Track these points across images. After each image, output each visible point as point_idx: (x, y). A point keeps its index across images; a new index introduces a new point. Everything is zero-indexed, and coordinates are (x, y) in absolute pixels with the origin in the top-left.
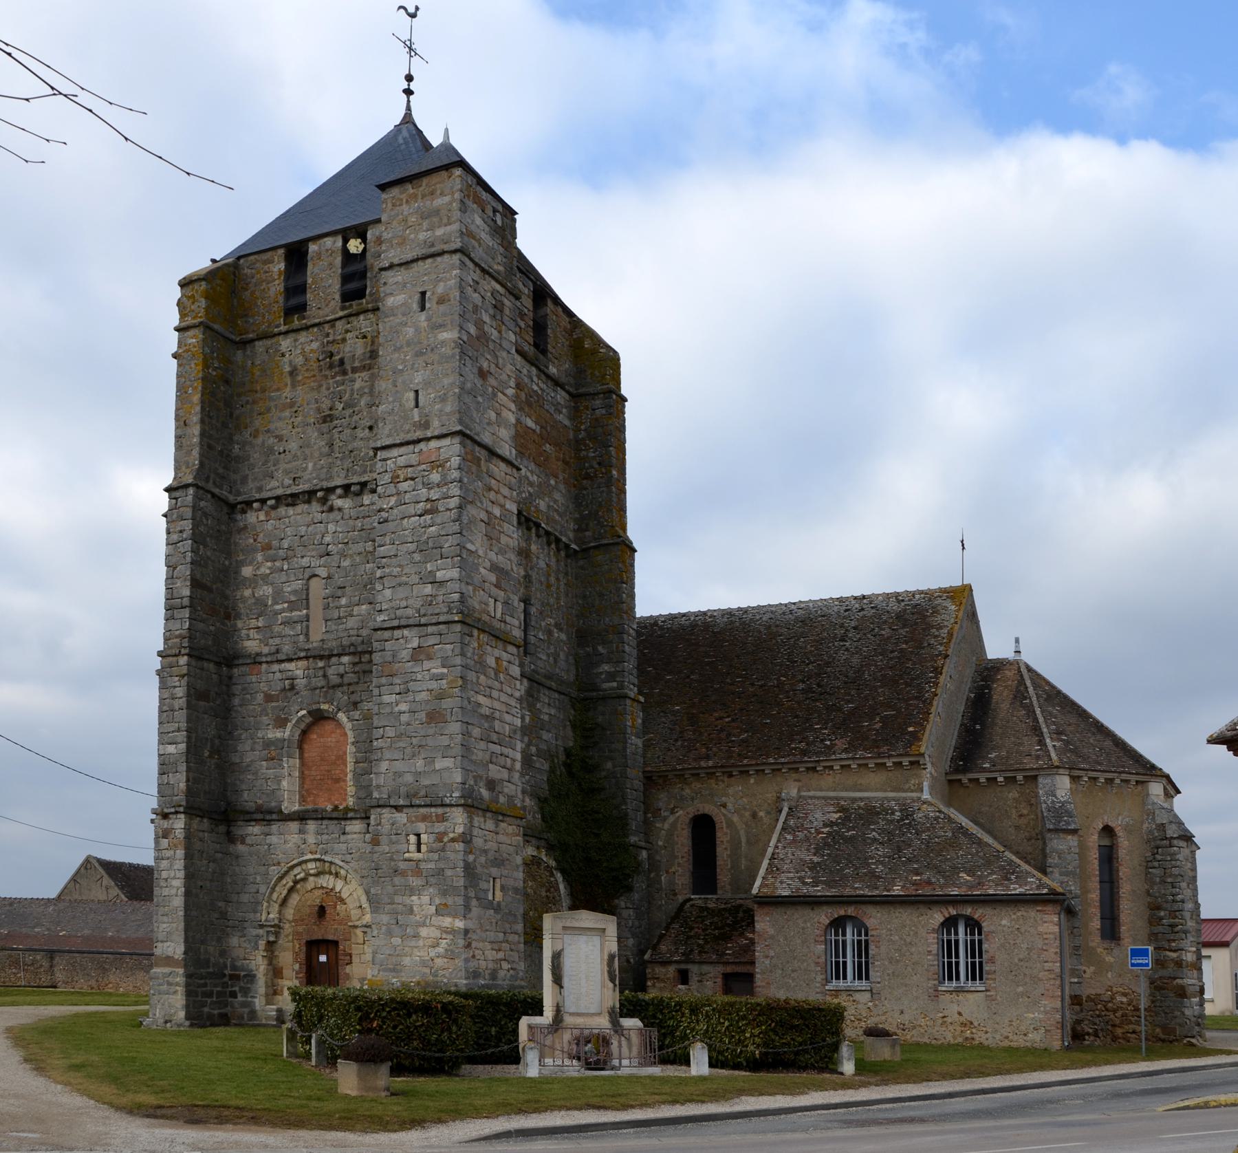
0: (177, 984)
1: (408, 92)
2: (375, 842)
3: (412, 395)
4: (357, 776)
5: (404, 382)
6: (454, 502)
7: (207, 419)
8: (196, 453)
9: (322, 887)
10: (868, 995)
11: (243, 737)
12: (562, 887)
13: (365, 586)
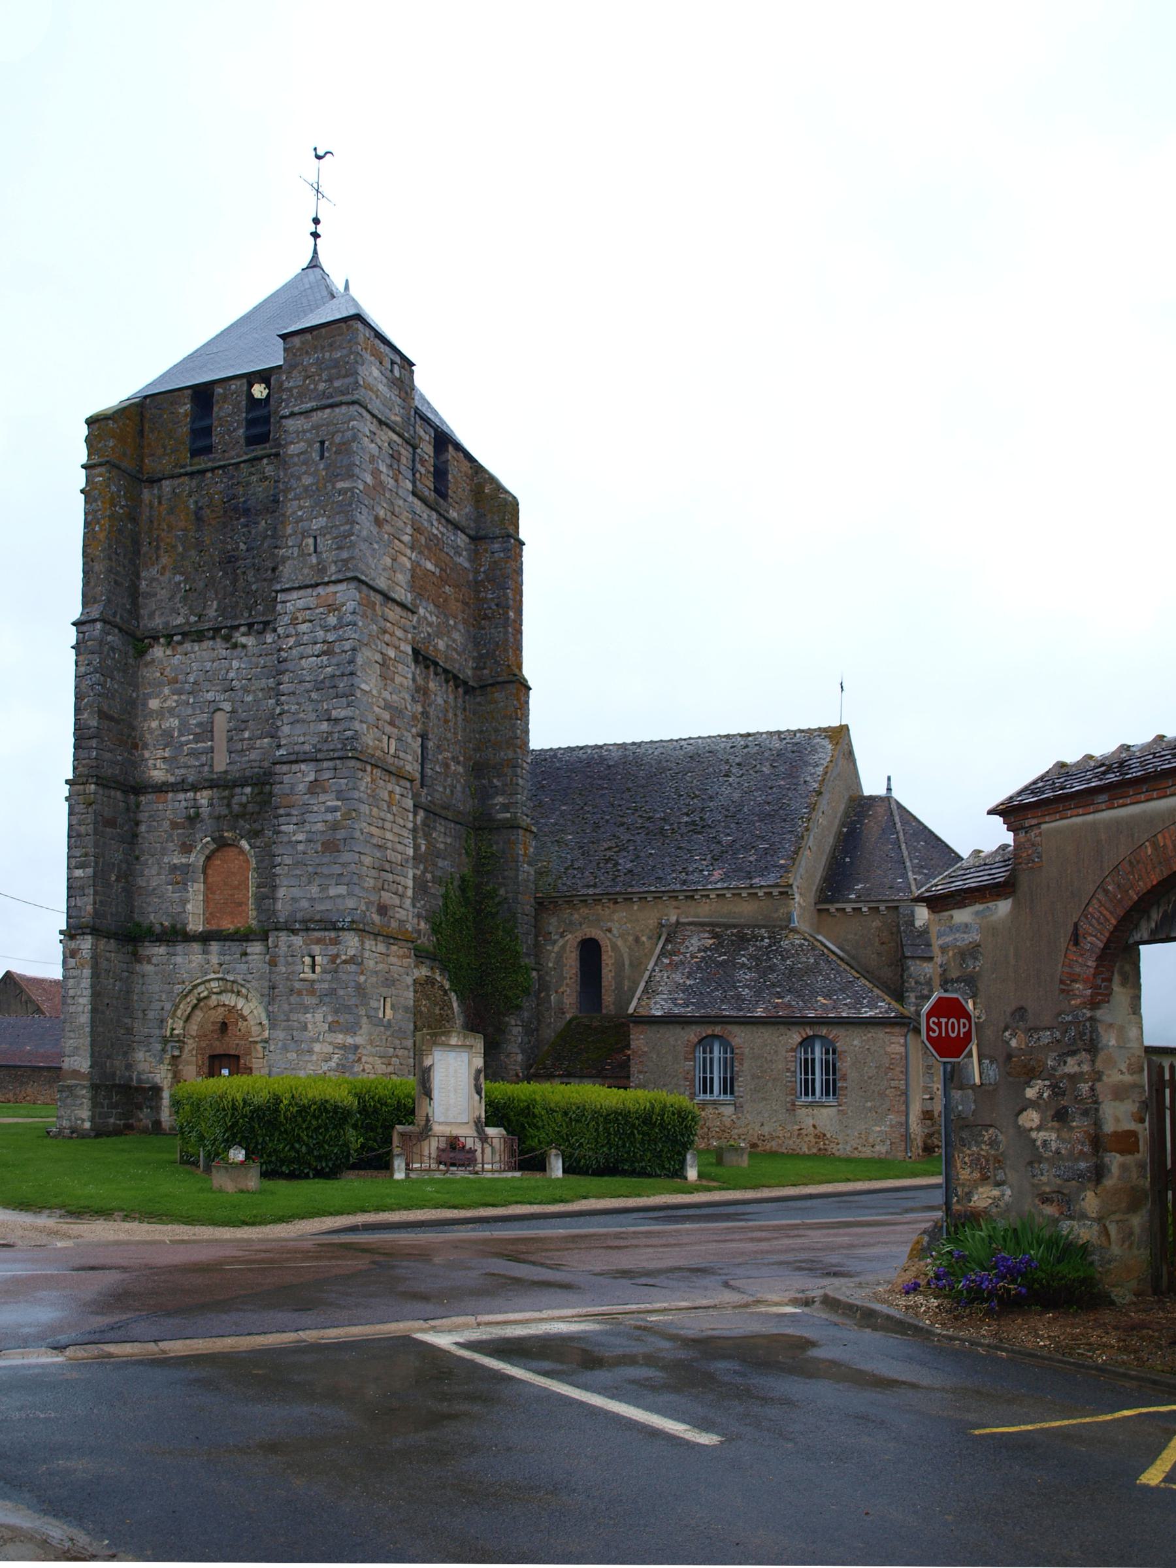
1: (315, 235)
2: (273, 963)
3: (311, 541)
7: (114, 556)
9: (224, 1005)
10: (731, 1109)
11: (150, 862)
12: (455, 1005)
13: (267, 720)
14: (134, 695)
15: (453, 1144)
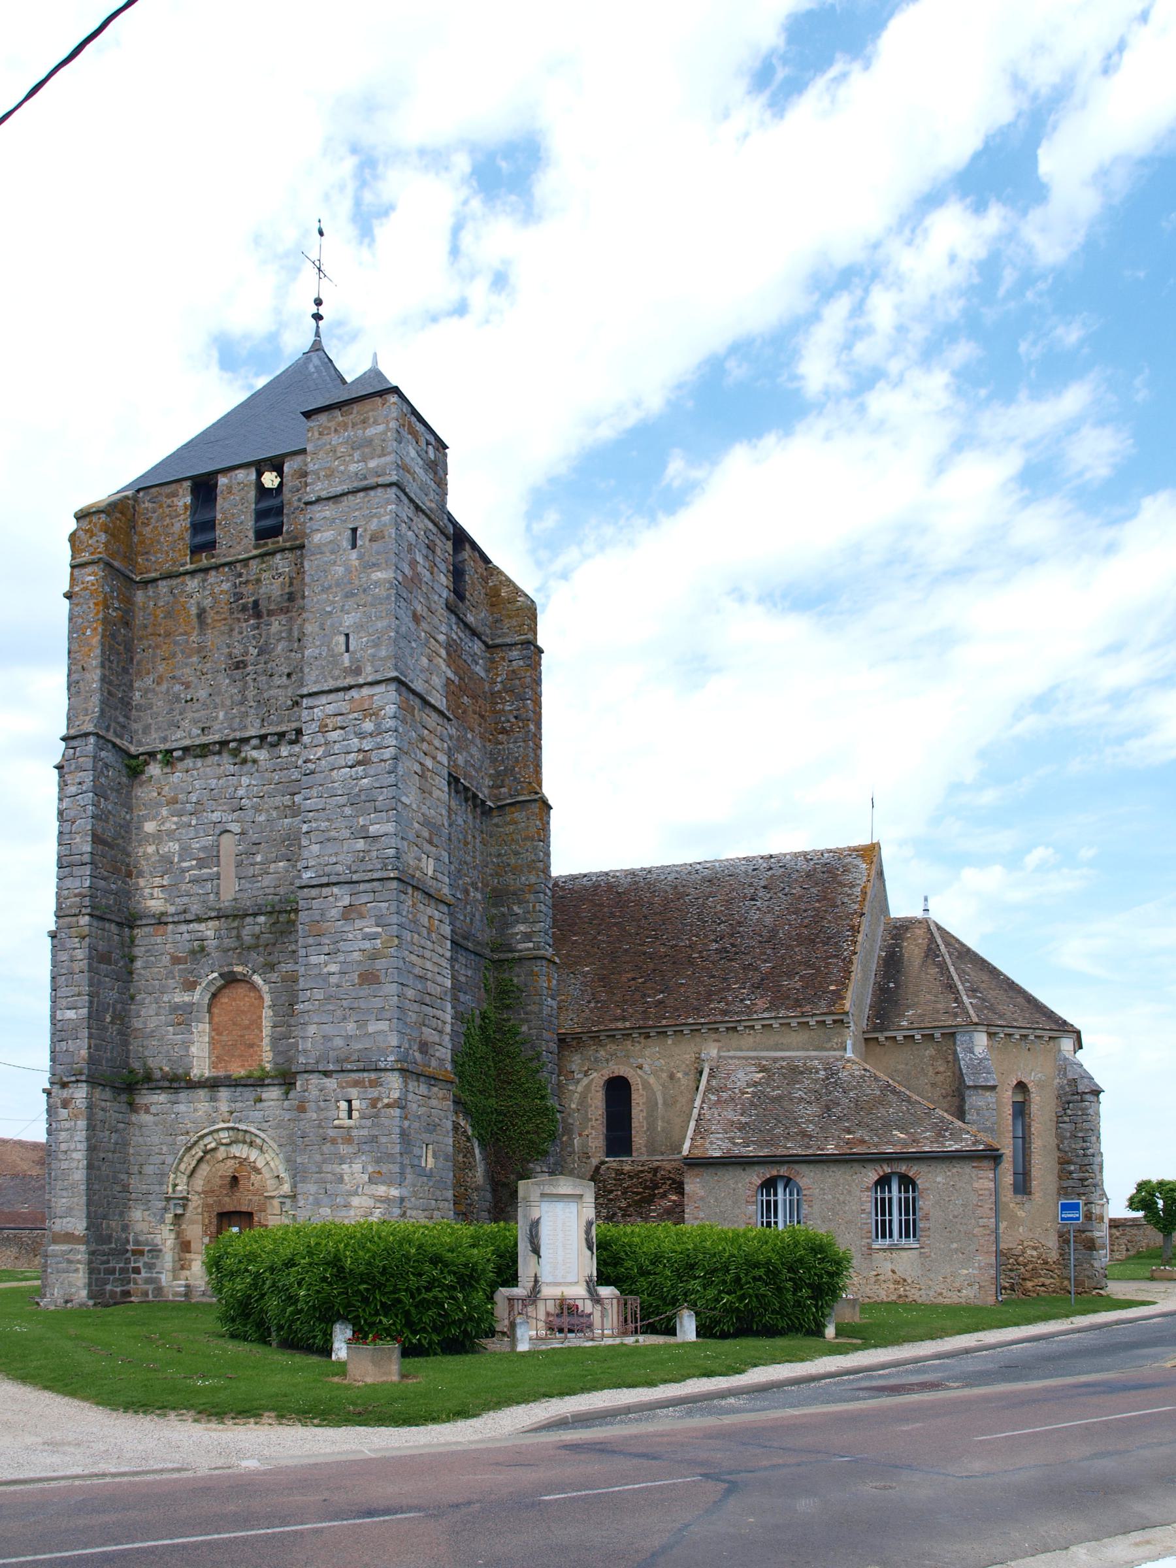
0: (79, 1262)
1: (318, 317)
2: (302, 1109)
3: (342, 639)
4: (275, 1041)
5: (332, 625)
6: (388, 753)
8: (96, 700)
9: (235, 1157)
12: (477, 1151)
14: (128, 817)
15: (566, 1308)
